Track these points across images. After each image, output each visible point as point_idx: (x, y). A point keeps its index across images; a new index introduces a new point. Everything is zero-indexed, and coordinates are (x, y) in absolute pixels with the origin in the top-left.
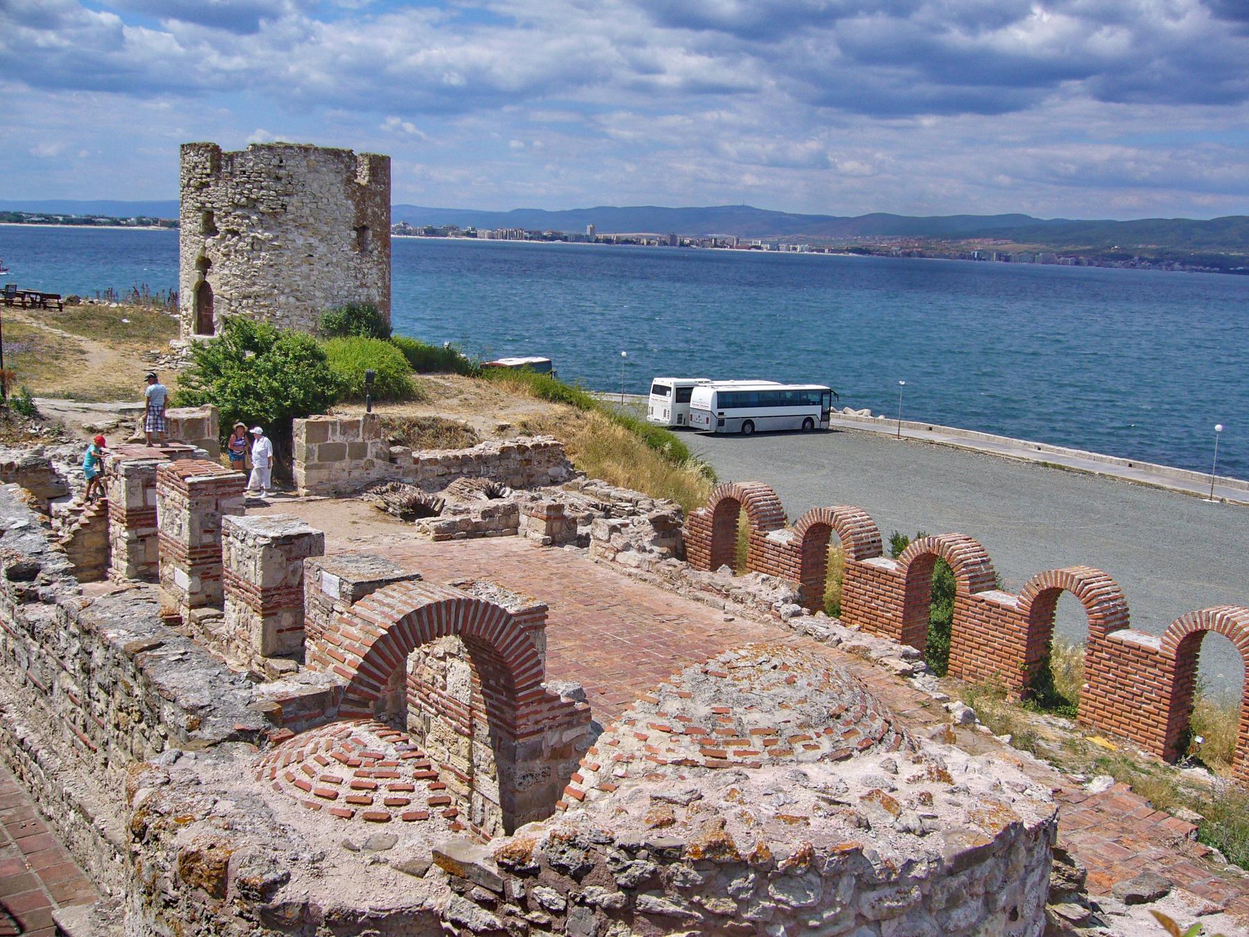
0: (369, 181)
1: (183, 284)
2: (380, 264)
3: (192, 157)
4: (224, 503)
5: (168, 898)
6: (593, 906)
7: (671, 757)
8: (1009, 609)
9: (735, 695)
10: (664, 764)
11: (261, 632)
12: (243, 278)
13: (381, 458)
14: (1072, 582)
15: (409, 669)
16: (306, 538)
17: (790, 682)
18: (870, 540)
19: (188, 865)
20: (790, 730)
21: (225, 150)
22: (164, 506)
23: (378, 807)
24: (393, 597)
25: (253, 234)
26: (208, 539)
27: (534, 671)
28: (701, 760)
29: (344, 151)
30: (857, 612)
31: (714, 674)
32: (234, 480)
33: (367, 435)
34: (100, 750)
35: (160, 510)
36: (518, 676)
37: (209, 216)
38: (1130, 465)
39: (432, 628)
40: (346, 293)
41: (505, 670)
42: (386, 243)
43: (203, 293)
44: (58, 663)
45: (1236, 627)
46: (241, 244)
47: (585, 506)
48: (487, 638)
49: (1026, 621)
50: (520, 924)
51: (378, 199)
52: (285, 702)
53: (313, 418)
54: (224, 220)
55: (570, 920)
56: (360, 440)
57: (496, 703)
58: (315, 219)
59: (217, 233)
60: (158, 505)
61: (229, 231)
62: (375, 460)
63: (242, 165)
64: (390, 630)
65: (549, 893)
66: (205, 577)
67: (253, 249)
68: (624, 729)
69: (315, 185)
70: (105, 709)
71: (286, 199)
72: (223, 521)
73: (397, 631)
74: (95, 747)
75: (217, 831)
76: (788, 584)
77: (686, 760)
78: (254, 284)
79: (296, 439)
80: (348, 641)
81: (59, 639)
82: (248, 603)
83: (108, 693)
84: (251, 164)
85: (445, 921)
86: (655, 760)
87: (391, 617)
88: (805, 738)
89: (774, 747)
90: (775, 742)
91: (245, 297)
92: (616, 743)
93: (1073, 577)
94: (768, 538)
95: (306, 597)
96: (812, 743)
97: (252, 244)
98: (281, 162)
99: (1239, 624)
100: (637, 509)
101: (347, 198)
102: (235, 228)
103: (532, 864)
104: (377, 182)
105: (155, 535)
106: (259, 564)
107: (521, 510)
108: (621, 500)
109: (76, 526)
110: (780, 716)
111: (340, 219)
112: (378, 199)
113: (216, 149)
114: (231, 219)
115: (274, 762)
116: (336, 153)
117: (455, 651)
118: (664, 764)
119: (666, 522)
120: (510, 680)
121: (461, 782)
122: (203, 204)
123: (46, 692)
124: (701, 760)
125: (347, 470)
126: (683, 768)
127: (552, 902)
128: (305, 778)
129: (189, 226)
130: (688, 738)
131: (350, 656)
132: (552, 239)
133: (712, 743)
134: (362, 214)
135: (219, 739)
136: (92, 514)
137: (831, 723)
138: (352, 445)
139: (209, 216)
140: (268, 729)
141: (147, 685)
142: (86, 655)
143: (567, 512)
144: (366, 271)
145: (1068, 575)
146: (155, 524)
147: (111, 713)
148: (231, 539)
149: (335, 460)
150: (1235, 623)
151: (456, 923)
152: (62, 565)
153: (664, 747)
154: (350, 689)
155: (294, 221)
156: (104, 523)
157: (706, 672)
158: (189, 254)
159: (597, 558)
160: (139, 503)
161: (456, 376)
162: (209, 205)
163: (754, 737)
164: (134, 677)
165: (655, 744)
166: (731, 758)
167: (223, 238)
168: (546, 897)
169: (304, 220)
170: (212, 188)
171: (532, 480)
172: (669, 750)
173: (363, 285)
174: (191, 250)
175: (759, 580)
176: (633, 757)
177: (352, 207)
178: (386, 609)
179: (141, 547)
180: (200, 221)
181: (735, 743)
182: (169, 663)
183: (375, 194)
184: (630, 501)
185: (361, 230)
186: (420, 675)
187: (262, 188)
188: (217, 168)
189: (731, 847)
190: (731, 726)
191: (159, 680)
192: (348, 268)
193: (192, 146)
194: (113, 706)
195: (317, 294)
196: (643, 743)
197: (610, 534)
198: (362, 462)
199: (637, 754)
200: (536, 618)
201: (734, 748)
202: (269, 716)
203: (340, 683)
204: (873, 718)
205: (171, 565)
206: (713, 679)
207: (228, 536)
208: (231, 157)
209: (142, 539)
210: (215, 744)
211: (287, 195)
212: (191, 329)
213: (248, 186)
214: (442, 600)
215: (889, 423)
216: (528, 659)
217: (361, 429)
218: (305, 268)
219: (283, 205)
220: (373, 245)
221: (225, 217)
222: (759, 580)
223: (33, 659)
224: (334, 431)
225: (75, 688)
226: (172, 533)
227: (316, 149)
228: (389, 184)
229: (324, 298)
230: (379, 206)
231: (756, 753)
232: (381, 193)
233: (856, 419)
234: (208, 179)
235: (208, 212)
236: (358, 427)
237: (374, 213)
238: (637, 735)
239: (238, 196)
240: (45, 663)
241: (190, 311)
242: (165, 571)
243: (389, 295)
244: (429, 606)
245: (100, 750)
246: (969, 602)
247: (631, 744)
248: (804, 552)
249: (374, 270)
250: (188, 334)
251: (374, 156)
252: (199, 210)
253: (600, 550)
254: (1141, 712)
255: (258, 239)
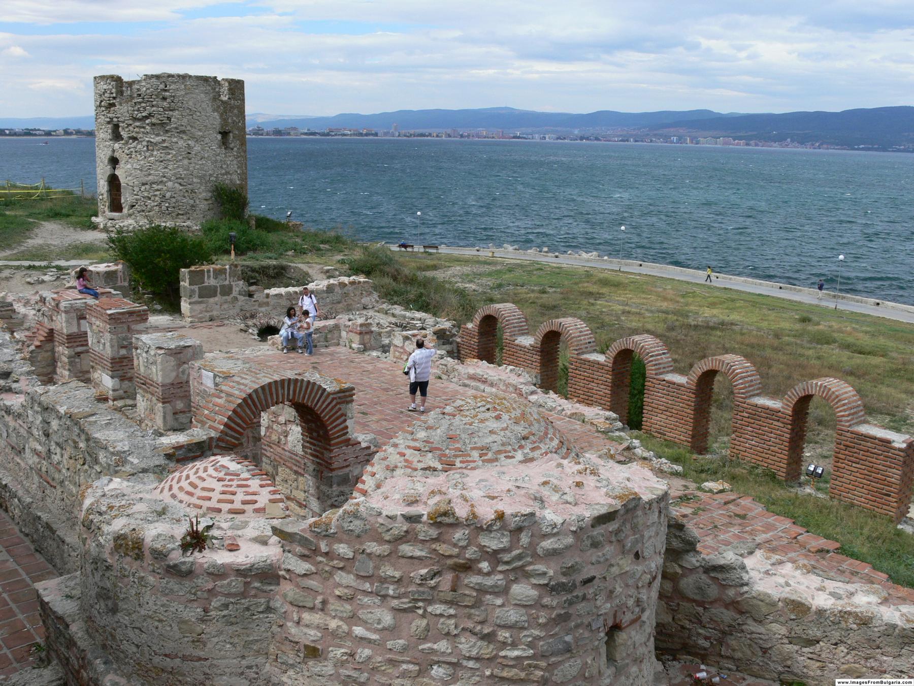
0: (229, 98)
1: (99, 176)
2: (239, 157)
3: (103, 86)
4: (135, 327)
5: (107, 564)
6: (369, 555)
7: (420, 465)
8: (680, 385)
9: (461, 427)
10: (416, 470)
11: (162, 414)
12: (141, 170)
13: (242, 295)
14: (723, 365)
15: (263, 433)
16: (190, 350)
17: (498, 418)
18: (587, 341)
19: (119, 542)
20: (495, 447)
21: (125, 79)
22: (92, 331)
23: (237, 505)
24: (246, 379)
25: (147, 139)
26: (123, 352)
27: (342, 426)
28: (440, 467)
29: (210, 77)
30: (580, 392)
31: (449, 414)
32: (139, 311)
33: (232, 278)
34: (58, 487)
35: (89, 334)
36: (332, 429)
37: (116, 127)
38: (781, 288)
39: (272, 399)
40: (215, 179)
41: (323, 426)
42: (243, 142)
43: (114, 182)
44: (28, 432)
45: (830, 392)
46: (139, 146)
47: (388, 324)
48: (309, 404)
49: (693, 393)
50: (327, 568)
51: (236, 111)
52: (178, 448)
53: (193, 268)
54: (127, 130)
55: (357, 563)
56: (227, 283)
57: (318, 449)
58: (191, 126)
59: (122, 139)
60: (89, 330)
61: (130, 138)
62: (239, 297)
63: (138, 90)
64: (244, 400)
65: (344, 548)
66: (123, 378)
67: (148, 150)
68: (391, 450)
69: (191, 103)
70: (60, 459)
71: (171, 113)
72: (134, 340)
73: (249, 401)
74: (55, 485)
75: (137, 521)
76: (528, 373)
77: (430, 467)
78: (150, 175)
79: (182, 283)
80: (217, 408)
81: (27, 416)
82: (153, 394)
83: (62, 448)
84: (144, 89)
85: (281, 570)
86: (410, 467)
87: (245, 391)
88: (506, 452)
89: (486, 458)
90: (486, 454)
91: (143, 184)
92: (385, 459)
93: (723, 361)
94: (516, 342)
95: (192, 388)
96: (510, 454)
97: (147, 146)
98: (166, 87)
99: (833, 390)
100: (424, 325)
101: (214, 111)
102: (134, 135)
103: (332, 531)
104: (235, 99)
105: (87, 352)
106: (159, 367)
107: (342, 328)
108: (413, 319)
109: (32, 348)
110: (490, 439)
111: (209, 126)
112: (236, 111)
113: (118, 80)
114: (131, 128)
115: (171, 481)
116: (205, 79)
117: (292, 419)
118: (416, 470)
119: (445, 333)
120: (326, 432)
121: (300, 507)
122: (111, 119)
123: (20, 452)
124: (440, 467)
125: (219, 303)
126: (428, 471)
127: (345, 554)
128: (190, 489)
129: (102, 136)
130: (430, 455)
131: (220, 417)
132: (366, 135)
133: (445, 455)
134: (224, 120)
135: (135, 471)
136: (43, 339)
137: (523, 442)
138: (222, 287)
139: (116, 127)
140: (167, 465)
141: (88, 440)
142: (46, 425)
143: (374, 329)
144: (229, 162)
145: (720, 360)
146: (87, 345)
147: (65, 461)
148: (139, 351)
149: (210, 297)
150: (830, 389)
151: (288, 571)
152: (26, 369)
153: (416, 460)
154: (219, 439)
155: (176, 128)
156: (51, 344)
157: (444, 414)
158: (103, 154)
159: (395, 360)
160: (74, 329)
161: (810, 404)
162: (115, 120)
163: (474, 451)
164: (79, 435)
165: (410, 459)
166: (458, 465)
167: (127, 143)
168: (341, 551)
169: (183, 128)
170: (118, 107)
171: (350, 307)
172: (419, 461)
173: (227, 173)
174: (104, 153)
175: (508, 370)
176: (396, 467)
177: (218, 117)
178: (242, 387)
179: (77, 360)
180: (110, 131)
181: (460, 456)
182: (101, 425)
183: (232, 108)
184: (420, 320)
185: (224, 134)
186: (270, 437)
187: (153, 106)
188: (120, 93)
189: (453, 514)
190: (457, 445)
191: (97, 435)
192: (216, 161)
193: (102, 78)
194: (66, 456)
195: (195, 180)
196: (403, 458)
197: (404, 342)
198: (229, 298)
199: (399, 465)
200: (345, 396)
201: (461, 459)
202: (169, 457)
203: (213, 435)
204: (552, 439)
205: (99, 372)
206: (447, 417)
207: (137, 349)
208: (131, 84)
209: (78, 354)
210: (133, 475)
211: (171, 110)
212: (106, 209)
213: (143, 105)
214: (278, 379)
215: (611, 262)
216: (337, 418)
217: (228, 275)
218: (186, 162)
219: (168, 118)
220: (234, 144)
221: (127, 127)
222: (508, 370)
223: (10, 431)
224: (209, 277)
225: (39, 448)
226: (98, 348)
227: (190, 77)
228: (243, 100)
229: (199, 183)
230: (238, 117)
231: (474, 461)
232: (238, 107)
233: (588, 261)
234: (114, 101)
235: (115, 125)
236: (225, 273)
237: (234, 122)
238: (399, 453)
239: (136, 112)
240: (19, 433)
241: (105, 196)
242: (95, 375)
243: (246, 179)
244: (270, 384)
245: (58, 487)
246: (654, 381)
247: (394, 459)
248: (541, 352)
249: (235, 162)
250: (104, 212)
251: (232, 80)
252: (109, 123)
253: (397, 354)
254: (769, 452)
255: (151, 142)
